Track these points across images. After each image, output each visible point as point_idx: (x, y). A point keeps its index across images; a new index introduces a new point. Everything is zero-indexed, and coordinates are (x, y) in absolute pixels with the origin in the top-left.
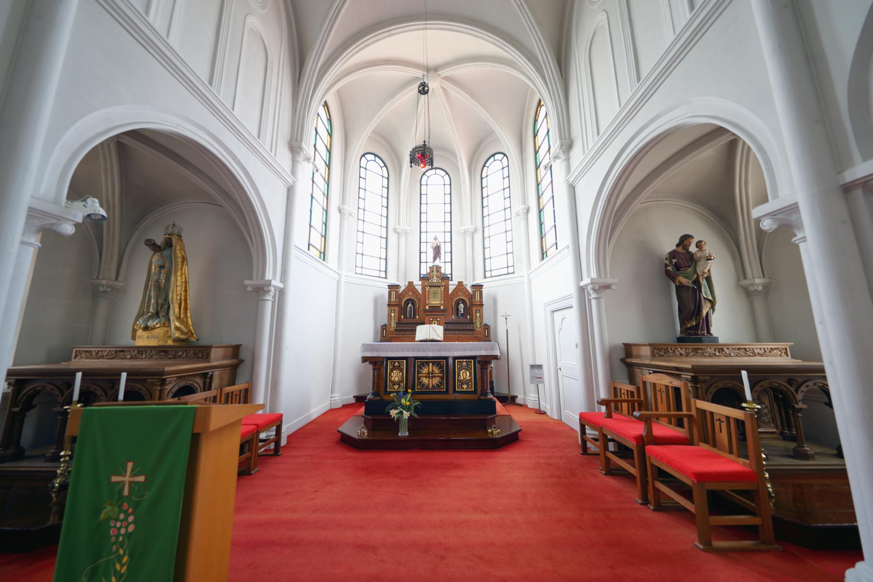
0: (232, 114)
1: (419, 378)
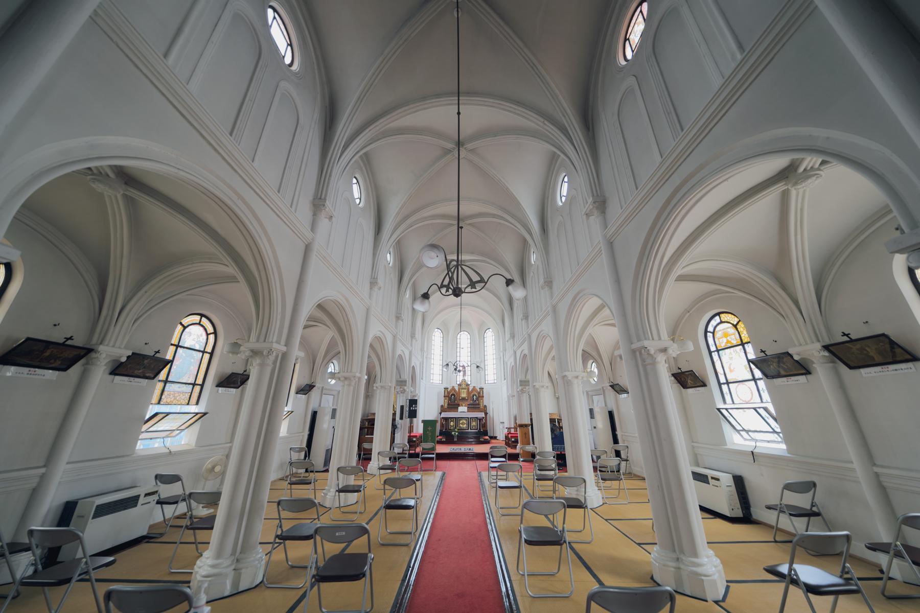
0: (252, 166)
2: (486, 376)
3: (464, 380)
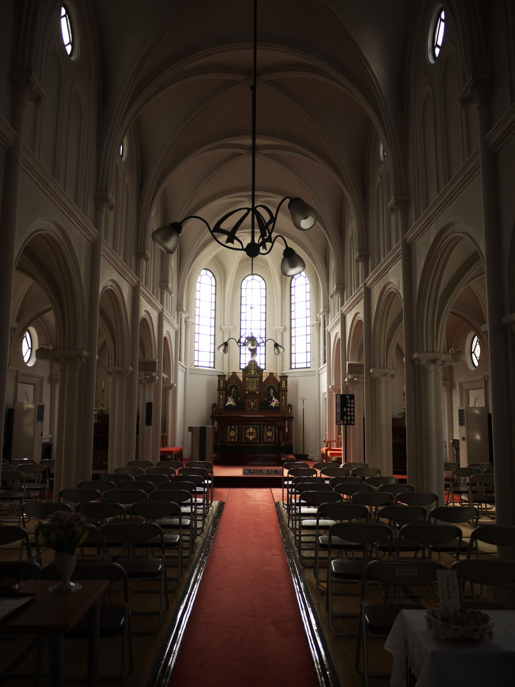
1: (245, 435)
2: (293, 355)
3: (253, 364)
